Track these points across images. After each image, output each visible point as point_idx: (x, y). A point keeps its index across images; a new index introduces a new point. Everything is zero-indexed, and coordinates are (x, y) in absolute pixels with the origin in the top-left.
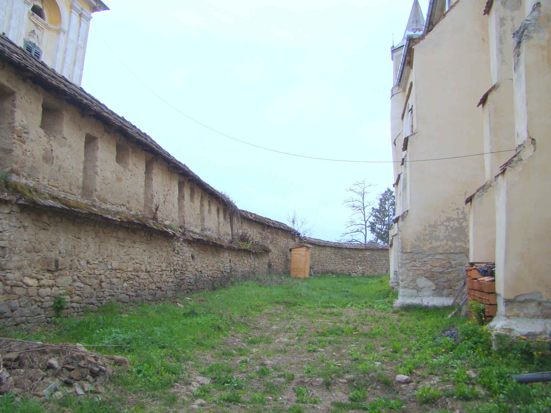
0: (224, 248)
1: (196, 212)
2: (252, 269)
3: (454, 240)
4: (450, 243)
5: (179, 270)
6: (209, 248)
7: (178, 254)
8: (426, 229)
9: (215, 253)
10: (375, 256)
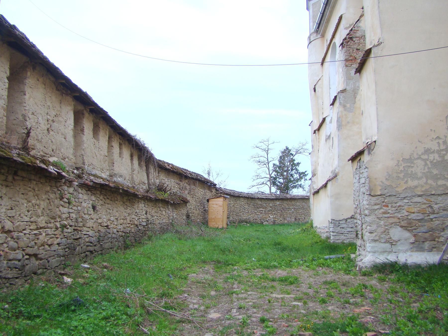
0: (139, 198)
1: (101, 152)
2: (171, 221)
3: (436, 178)
4: (430, 182)
5: (71, 226)
6: (119, 198)
7: (69, 203)
8: (400, 164)
9: (128, 204)
10: (284, 205)
